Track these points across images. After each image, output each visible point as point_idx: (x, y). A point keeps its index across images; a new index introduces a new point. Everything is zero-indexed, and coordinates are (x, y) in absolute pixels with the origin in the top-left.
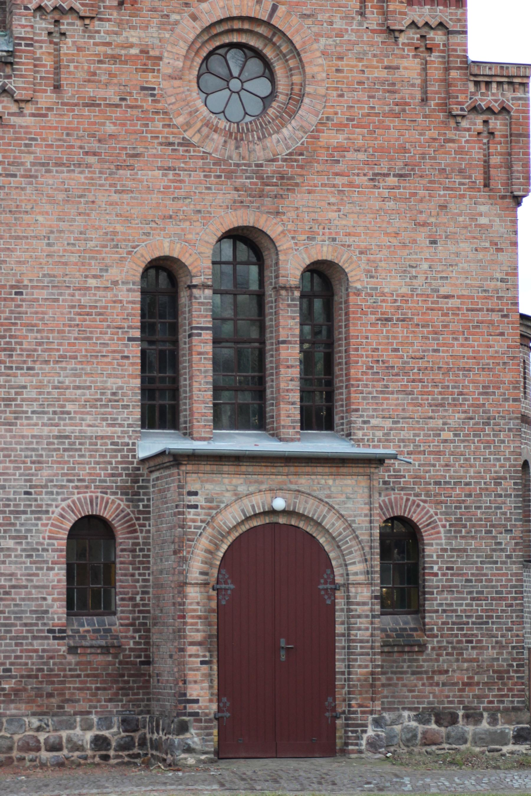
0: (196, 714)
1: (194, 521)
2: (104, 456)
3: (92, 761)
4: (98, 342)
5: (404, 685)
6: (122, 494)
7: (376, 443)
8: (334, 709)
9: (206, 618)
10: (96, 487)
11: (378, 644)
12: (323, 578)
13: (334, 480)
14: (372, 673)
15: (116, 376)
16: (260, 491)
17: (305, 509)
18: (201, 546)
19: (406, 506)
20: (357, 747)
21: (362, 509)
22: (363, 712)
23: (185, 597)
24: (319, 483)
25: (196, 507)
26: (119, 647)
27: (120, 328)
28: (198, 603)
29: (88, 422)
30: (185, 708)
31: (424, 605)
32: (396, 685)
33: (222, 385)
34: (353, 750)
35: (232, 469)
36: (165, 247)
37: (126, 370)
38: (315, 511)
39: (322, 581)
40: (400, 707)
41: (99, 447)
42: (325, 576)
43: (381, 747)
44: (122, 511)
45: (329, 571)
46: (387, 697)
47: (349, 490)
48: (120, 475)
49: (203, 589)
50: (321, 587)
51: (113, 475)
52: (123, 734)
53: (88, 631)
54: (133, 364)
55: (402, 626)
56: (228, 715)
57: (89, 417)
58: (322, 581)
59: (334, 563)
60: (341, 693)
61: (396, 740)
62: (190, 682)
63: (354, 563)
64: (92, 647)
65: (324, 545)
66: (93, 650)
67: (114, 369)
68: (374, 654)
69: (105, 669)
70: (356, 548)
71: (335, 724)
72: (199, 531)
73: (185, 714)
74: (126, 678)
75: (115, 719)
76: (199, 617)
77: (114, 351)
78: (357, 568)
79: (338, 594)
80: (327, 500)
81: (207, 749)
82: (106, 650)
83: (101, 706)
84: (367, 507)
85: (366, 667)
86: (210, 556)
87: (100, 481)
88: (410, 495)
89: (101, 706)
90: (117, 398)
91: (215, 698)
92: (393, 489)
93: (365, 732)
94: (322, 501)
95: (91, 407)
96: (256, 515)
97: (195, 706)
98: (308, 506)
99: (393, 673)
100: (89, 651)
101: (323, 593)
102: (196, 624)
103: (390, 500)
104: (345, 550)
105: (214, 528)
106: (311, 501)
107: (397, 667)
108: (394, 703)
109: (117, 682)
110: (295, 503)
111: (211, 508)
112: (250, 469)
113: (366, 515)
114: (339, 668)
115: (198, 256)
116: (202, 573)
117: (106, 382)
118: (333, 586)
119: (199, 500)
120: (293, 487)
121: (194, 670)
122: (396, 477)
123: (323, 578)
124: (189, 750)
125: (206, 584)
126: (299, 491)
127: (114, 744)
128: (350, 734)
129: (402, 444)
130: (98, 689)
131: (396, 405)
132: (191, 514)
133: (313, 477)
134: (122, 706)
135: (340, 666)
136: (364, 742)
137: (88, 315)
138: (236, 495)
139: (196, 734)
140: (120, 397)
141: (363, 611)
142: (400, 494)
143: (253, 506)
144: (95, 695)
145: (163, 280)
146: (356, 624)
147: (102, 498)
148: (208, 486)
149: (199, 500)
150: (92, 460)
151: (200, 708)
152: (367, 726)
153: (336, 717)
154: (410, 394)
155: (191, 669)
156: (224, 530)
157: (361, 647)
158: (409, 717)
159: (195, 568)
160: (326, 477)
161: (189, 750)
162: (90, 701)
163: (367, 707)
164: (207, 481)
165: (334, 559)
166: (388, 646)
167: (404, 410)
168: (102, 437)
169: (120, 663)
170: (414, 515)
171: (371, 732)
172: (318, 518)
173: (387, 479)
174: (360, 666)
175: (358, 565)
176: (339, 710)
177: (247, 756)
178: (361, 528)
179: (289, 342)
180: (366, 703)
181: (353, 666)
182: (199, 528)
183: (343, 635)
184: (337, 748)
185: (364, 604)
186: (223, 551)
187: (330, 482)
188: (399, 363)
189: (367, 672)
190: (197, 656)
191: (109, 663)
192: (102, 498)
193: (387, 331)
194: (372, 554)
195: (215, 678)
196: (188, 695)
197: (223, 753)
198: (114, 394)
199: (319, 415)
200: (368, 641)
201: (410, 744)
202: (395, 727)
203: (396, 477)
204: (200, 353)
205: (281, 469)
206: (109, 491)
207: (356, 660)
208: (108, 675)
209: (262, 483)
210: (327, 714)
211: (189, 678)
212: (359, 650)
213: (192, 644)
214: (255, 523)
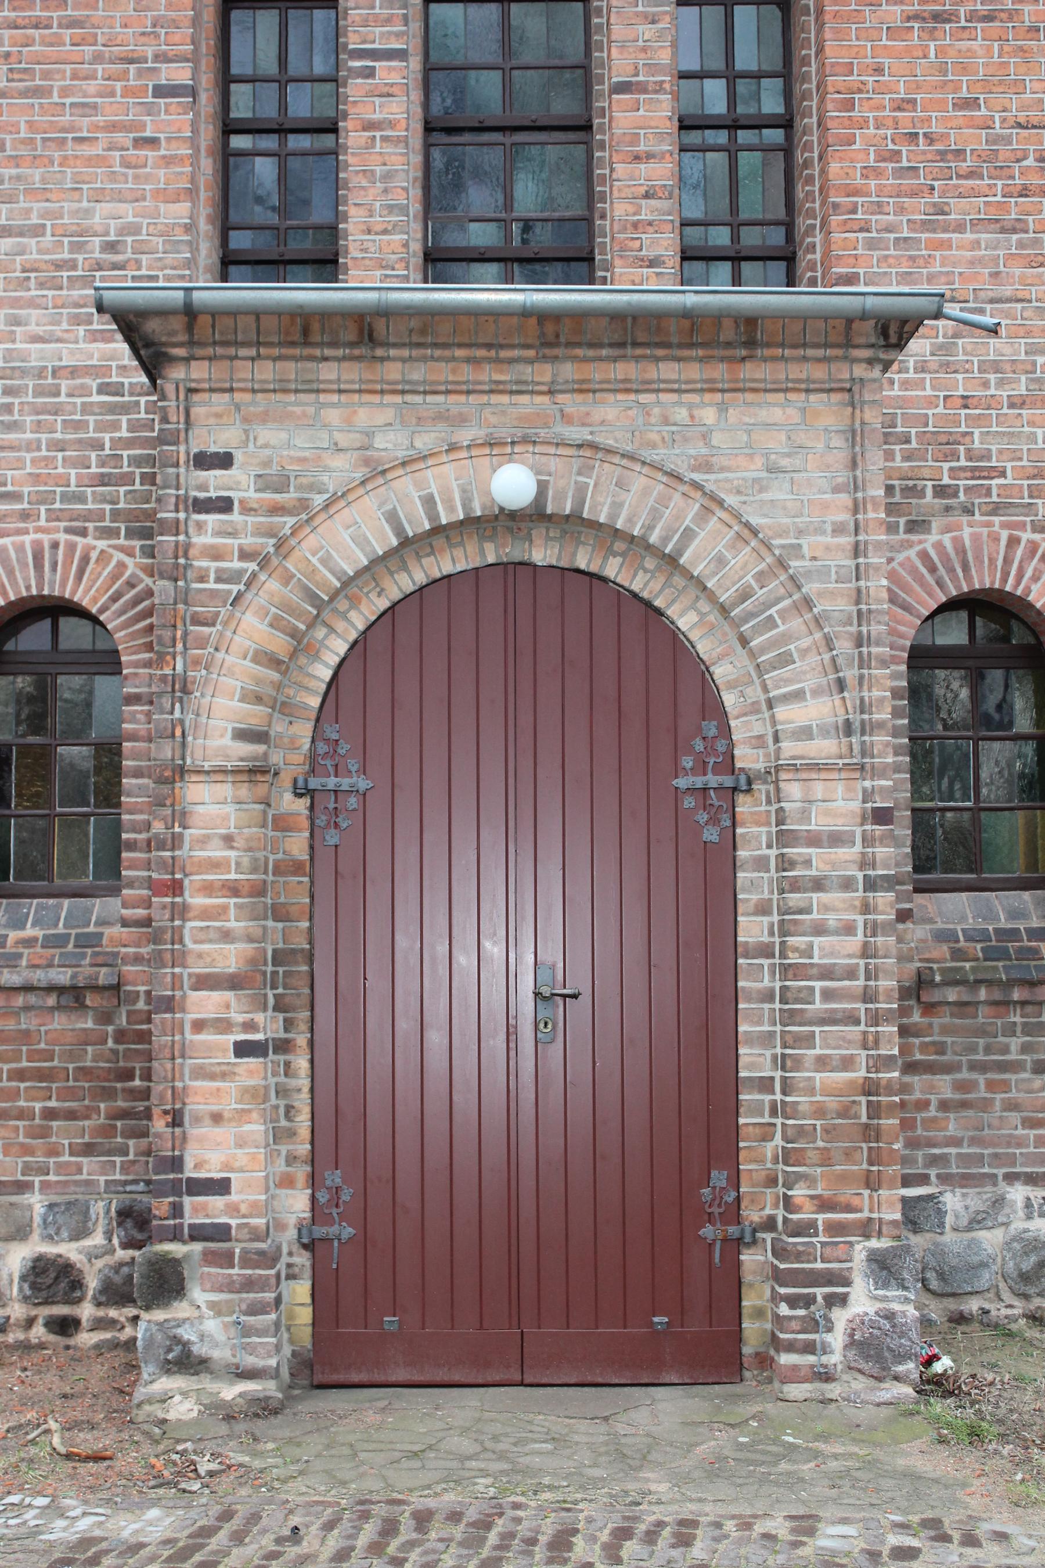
0: (222, 1233)
1: (216, 554)
2: (79, 426)
3: (21, 1336)
4: (68, 101)
5: (1012, 1106)
6: (130, 534)
7: (911, 375)
8: (733, 1213)
9: (259, 890)
10: (54, 516)
11: (887, 984)
12: (690, 750)
13: (722, 408)
14: (869, 1088)
15: (119, 197)
16: (453, 448)
17: (617, 506)
18: (240, 642)
19: (1007, 561)
20: (811, 1359)
21: (825, 506)
22: (835, 1229)
23: (183, 817)
24: (666, 421)
25: (224, 505)
26: (116, 988)
27: (131, 61)
28: (228, 840)
29: (33, 328)
30: (177, 1211)
32: (985, 1105)
34: (795, 1368)
35: (352, 373)
37: (147, 178)
38: (655, 515)
39: (687, 762)
40: (1000, 1172)
41: (63, 398)
42: (699, 745)
43: (901, 1357)
44: (131, 585)
45: (711, 729)
46: (957, 1142)
47: (777, 442)
48: (126, 479)
49: (244, 791)
50: (682, 783)
51: (103, 480)
52: (122, 1254)
53: (30, 942)
54: (168, 161)
55: (1004, 923)
56: (348, 1232)
57: (35, 313)
58: (687, 762)
59: (729, 699)
60: (759, 1156)
61: (985, 1279)
62: (197, 1120)
63: (798, 695)
64: (28, 988)
65: (694, 636)
66: (32, 999)
67: (112, 176)
68: (875, 1019)
69: (71, 1056)
70: (805, 642)
71: (738, 1264)
72: (235, 588)
73: (175, 1235)
74: (137, 1082)
75: (98, 1208)
76: (233, 889)
77: (113, 127)
78: (811, 712)
79: (744, 806)
80: (697, 477)
81: (251, 1361)
82: (72, 996)
83: (60, 1168)
84: (845, 499)
85: (847, 1063)
86: (275, 676)
87: (65, 498)
88: (1022, 526)
89: (60, 1168)
90: (119, 258)
91: (301, 1172)
92: (969, 511)
93: (843, 1300)
94: (679, 478)
95: (41, 285)
96: (441, 532)
97: (216, 1202)
98: (629, 499)
99: (973, 1067)
100: (20, 1000)
101: (689, 802)
102: (221, 912)
103: (958, 542)
104: (763, 650)
105: (287, 579)
106: (639, 482)
107: (988, 1050)
108: (980, 1159)
109: (109, 1094)
110: (581, 491)
111: (277, 510)
112: (418, 373)
113: (838, 529)
114: (751, 1067)
116: (242, 735)
117: (88, 213)
118: (728, 781)
119: (237, 482)
120: (576, 433)
121: (212, 1077)
122: (975, 473)
123: (690, 750)
124: (185, 1362)
125: (256, 772)
126: (594, 446)
127: (92, 1284)
128: (784, 1310)
129: (992, 377)
130: (50, 1114)
131: (972, 263)
132: (207, 531)
133: (643, 398)
134: (125, 1169)
135: (754, 1060)
136: (837, 1340)
137: (36, 27)
138: (366, 462)
139: (212, 1305)
140: (129, 255)
141: (834, 865)
142: (988, 525)
143: (429, 502)
144: (44, 1133)
146: (808, 911)
147: (71, 547)
148: (268, 435)
149: (237, 482)
150: (44, 437)
151: (233, 1210)
152: (847, 1283)
153: (737, 1244)
154: (1014, 231)
155: (201, 1073)
156: (324, 584)
157: (828, 995)
158: (1028, 1204)
160: (694, 398)
161: (185, 1362)
162: (27, 1150)
163: (849, 1208)
164: (264, 418)
165: (731, 685)
166: (956, 983)
167: (996, 275)
168: (74, 372)
169: (121, 1036)
170: (1035, 588)
171: (863, 1300)
172: (666, 539)
173: (946, 480)
174: (822, 1063)
175: (810, 701)
176: (752, 1215)
177: (417, 1378)
178: (823, 573)
179: (642, 88)
180: (846, 1194)
181: (798, 1063)
182: (233, 577)
183: (765, 951)
184: (747, 1350)
185: (836, 839)
186: (334, 660)
187: (709, 415)
188: (975, 141)
189: (852, 1082)
190: (223, 1025)
191: (85, 1039)
192: (71, 547)
193: (940, 51)
194: (863, 662)
195: (302, 1102)
196: (189, 1163)
197: (330, 1364)
198: (111, 247)
200: (851, 974)
201: (1031, 1290)
202: (982, 1234)
203: (975, 473)
204: (370, 126)
205: (527, 372)
206: (90, 525)
207: (808, 1040)
208: (84, 1072)
209: (462, 420)
210: (708, 1231)
211: (196, 1105)
212: (819, 1004)
213: (204, 982)
214: (448, 562)
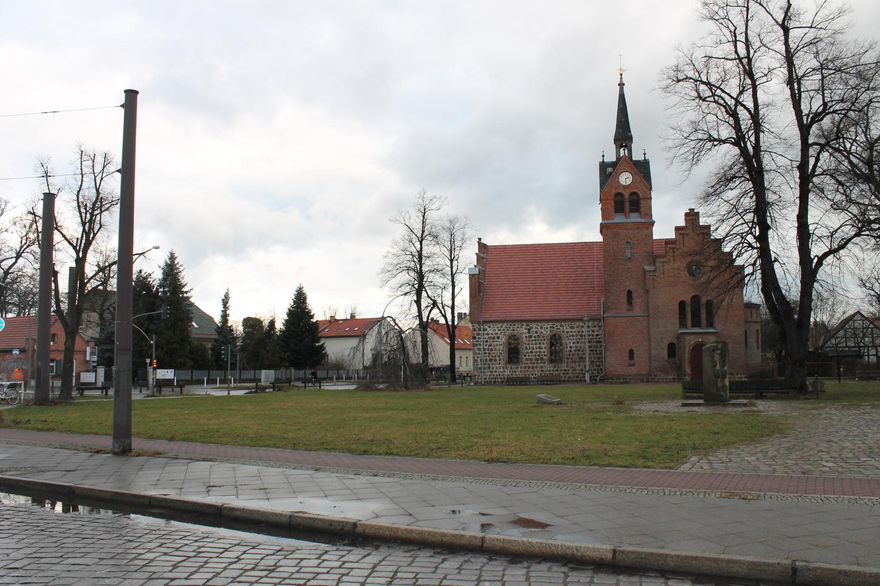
36: (683, 299)
145: (682, 304)
159: (687, 350)
199: (710, 324)
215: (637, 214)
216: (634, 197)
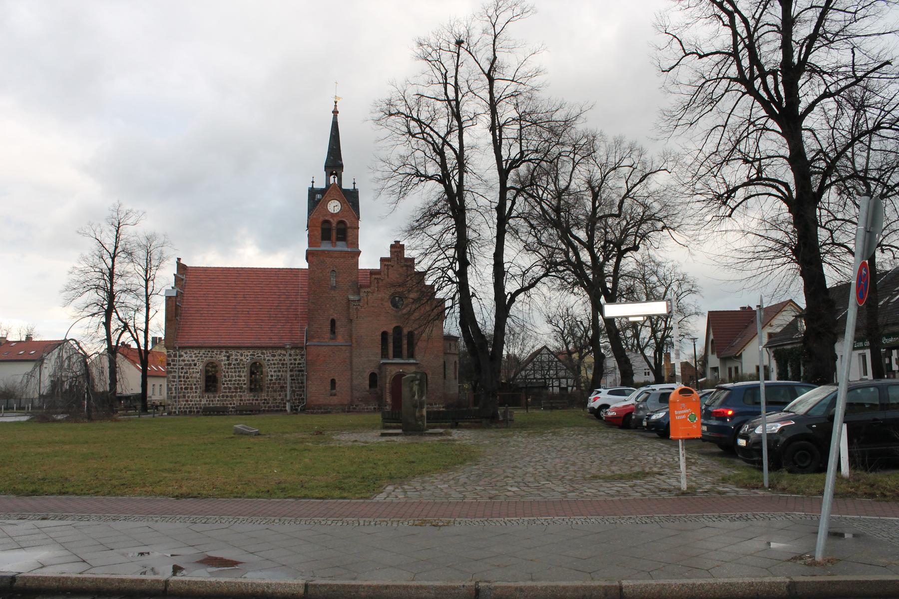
31: (103, 393)
33: (829, 16)
115: (391, 331)
145: (384, 335)
159: (388, 381)
199: (411, 355)
215: (343, 243)
216: (342, 226)
